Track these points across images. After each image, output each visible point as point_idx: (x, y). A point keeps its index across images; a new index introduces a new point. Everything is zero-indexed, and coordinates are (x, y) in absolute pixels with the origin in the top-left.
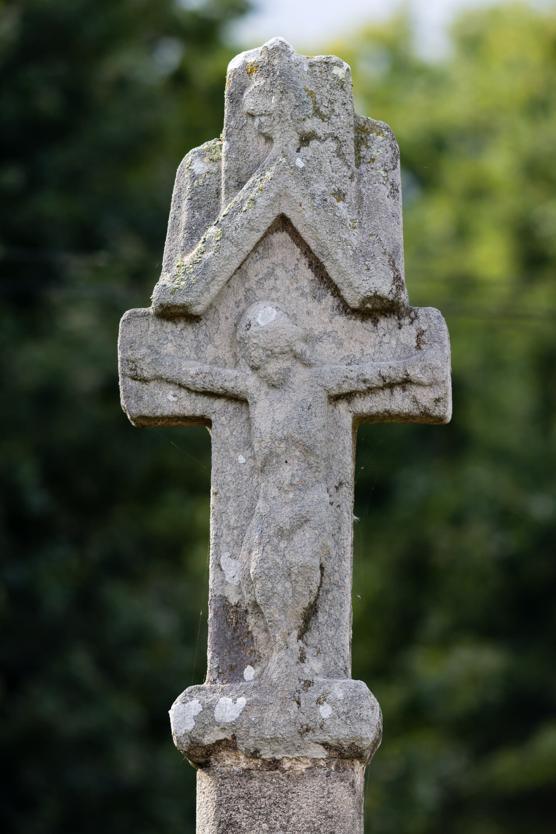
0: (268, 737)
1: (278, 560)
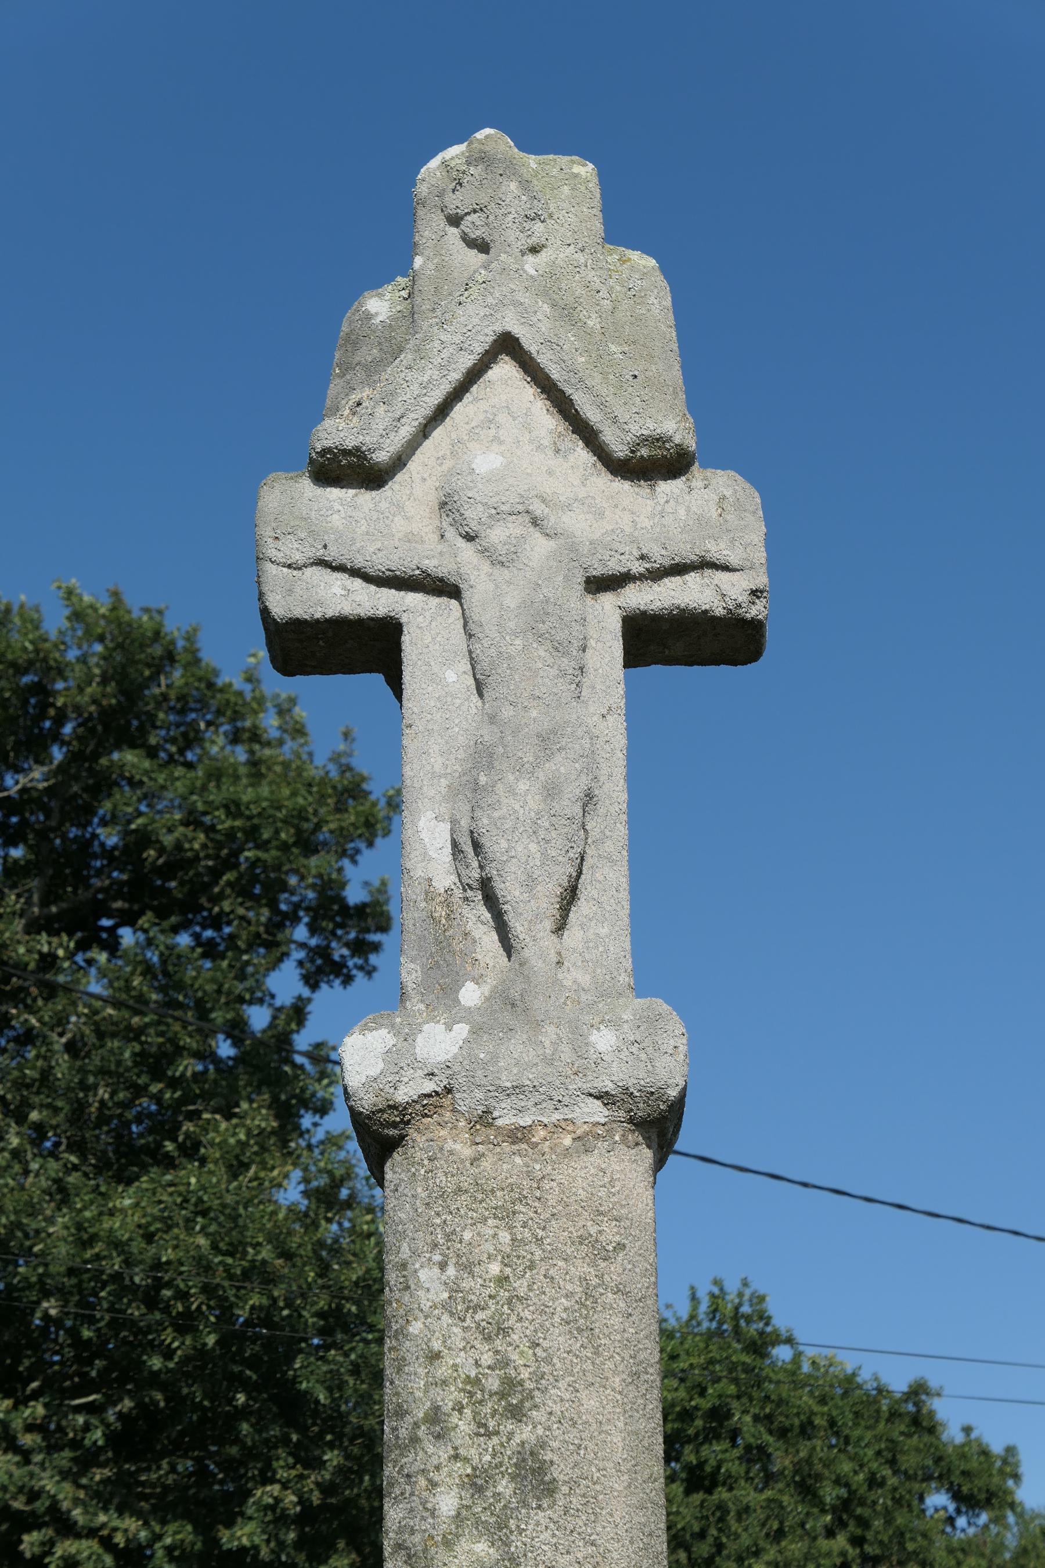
0: (509, 1085)
1: (517, 807)
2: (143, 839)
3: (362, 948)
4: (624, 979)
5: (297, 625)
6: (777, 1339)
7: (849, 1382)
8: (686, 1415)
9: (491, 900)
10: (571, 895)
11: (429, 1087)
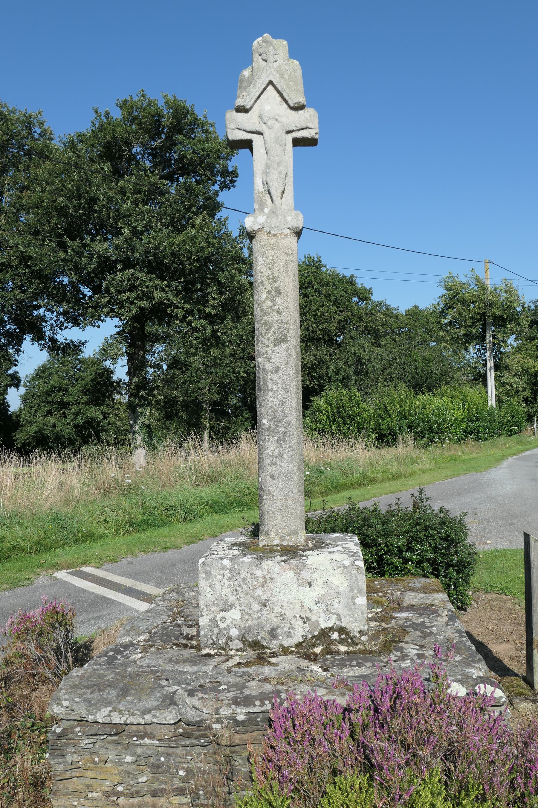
2: (184, 157)
3: (232, 181)
4: (293, 207)
5: (234, 141)
6: (323, 266)
7: (338, 275)
8: (303, 284)
9: (269, 193)
10: (283, 192)
11: (260, 227)
